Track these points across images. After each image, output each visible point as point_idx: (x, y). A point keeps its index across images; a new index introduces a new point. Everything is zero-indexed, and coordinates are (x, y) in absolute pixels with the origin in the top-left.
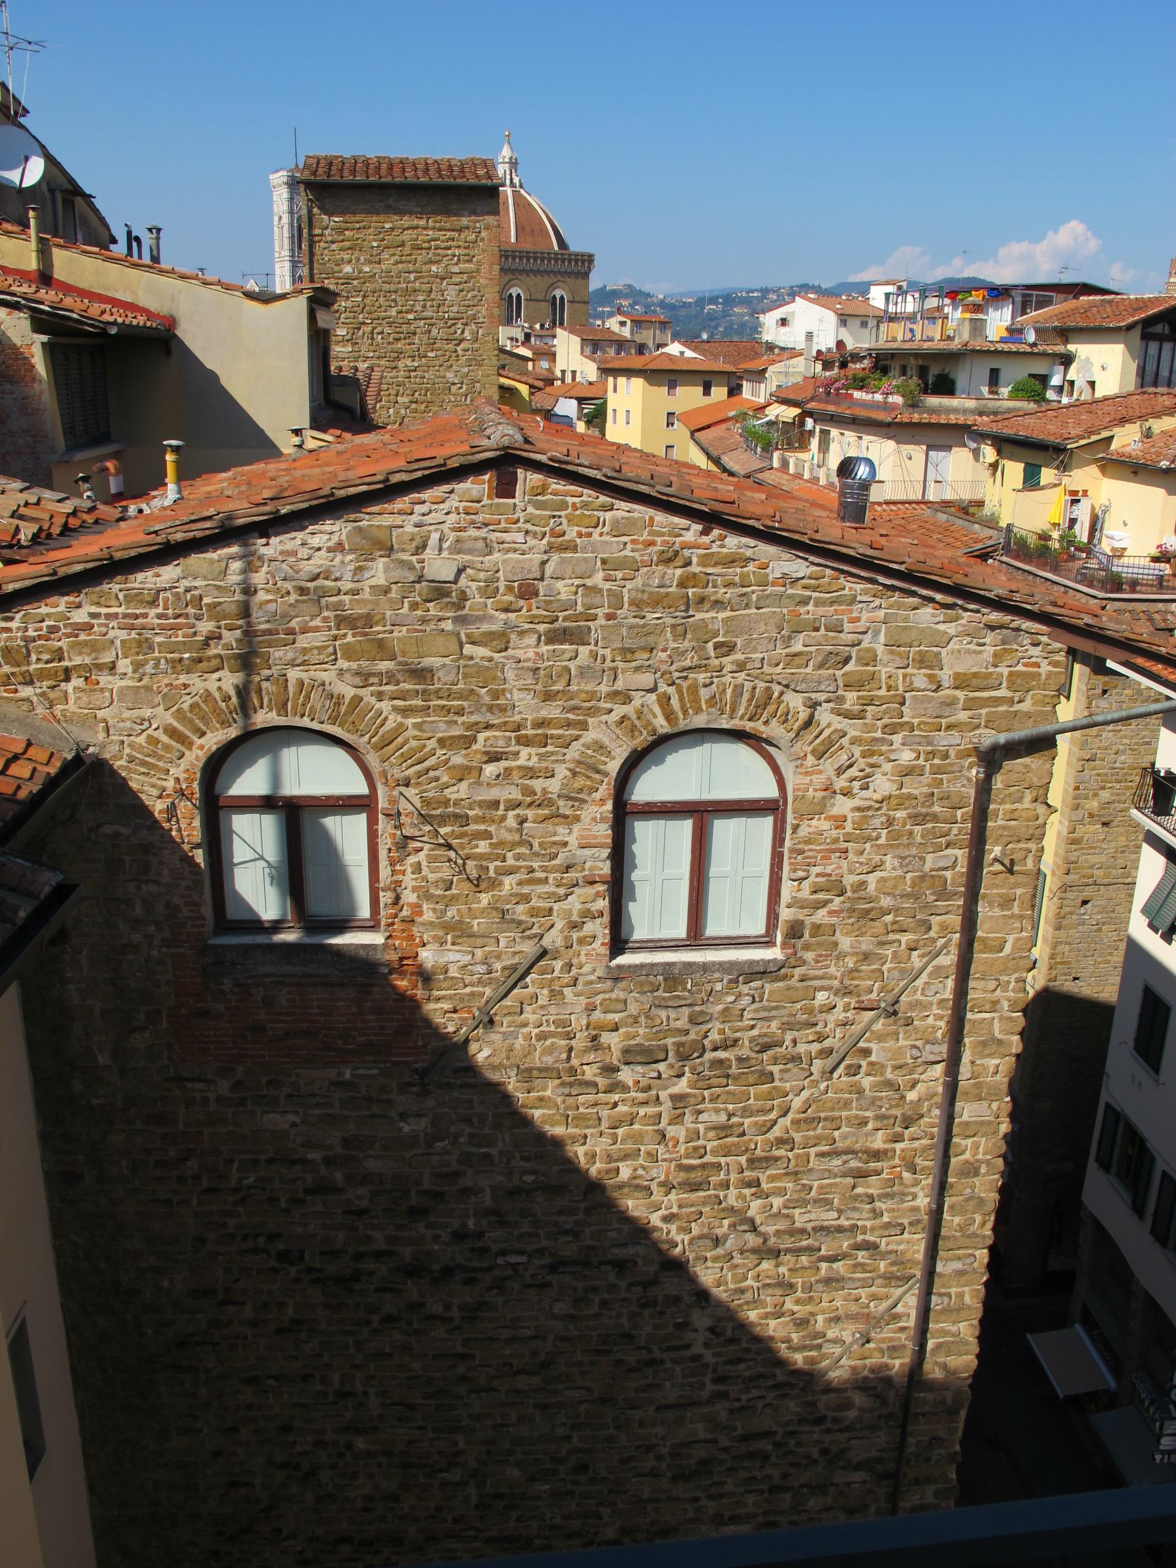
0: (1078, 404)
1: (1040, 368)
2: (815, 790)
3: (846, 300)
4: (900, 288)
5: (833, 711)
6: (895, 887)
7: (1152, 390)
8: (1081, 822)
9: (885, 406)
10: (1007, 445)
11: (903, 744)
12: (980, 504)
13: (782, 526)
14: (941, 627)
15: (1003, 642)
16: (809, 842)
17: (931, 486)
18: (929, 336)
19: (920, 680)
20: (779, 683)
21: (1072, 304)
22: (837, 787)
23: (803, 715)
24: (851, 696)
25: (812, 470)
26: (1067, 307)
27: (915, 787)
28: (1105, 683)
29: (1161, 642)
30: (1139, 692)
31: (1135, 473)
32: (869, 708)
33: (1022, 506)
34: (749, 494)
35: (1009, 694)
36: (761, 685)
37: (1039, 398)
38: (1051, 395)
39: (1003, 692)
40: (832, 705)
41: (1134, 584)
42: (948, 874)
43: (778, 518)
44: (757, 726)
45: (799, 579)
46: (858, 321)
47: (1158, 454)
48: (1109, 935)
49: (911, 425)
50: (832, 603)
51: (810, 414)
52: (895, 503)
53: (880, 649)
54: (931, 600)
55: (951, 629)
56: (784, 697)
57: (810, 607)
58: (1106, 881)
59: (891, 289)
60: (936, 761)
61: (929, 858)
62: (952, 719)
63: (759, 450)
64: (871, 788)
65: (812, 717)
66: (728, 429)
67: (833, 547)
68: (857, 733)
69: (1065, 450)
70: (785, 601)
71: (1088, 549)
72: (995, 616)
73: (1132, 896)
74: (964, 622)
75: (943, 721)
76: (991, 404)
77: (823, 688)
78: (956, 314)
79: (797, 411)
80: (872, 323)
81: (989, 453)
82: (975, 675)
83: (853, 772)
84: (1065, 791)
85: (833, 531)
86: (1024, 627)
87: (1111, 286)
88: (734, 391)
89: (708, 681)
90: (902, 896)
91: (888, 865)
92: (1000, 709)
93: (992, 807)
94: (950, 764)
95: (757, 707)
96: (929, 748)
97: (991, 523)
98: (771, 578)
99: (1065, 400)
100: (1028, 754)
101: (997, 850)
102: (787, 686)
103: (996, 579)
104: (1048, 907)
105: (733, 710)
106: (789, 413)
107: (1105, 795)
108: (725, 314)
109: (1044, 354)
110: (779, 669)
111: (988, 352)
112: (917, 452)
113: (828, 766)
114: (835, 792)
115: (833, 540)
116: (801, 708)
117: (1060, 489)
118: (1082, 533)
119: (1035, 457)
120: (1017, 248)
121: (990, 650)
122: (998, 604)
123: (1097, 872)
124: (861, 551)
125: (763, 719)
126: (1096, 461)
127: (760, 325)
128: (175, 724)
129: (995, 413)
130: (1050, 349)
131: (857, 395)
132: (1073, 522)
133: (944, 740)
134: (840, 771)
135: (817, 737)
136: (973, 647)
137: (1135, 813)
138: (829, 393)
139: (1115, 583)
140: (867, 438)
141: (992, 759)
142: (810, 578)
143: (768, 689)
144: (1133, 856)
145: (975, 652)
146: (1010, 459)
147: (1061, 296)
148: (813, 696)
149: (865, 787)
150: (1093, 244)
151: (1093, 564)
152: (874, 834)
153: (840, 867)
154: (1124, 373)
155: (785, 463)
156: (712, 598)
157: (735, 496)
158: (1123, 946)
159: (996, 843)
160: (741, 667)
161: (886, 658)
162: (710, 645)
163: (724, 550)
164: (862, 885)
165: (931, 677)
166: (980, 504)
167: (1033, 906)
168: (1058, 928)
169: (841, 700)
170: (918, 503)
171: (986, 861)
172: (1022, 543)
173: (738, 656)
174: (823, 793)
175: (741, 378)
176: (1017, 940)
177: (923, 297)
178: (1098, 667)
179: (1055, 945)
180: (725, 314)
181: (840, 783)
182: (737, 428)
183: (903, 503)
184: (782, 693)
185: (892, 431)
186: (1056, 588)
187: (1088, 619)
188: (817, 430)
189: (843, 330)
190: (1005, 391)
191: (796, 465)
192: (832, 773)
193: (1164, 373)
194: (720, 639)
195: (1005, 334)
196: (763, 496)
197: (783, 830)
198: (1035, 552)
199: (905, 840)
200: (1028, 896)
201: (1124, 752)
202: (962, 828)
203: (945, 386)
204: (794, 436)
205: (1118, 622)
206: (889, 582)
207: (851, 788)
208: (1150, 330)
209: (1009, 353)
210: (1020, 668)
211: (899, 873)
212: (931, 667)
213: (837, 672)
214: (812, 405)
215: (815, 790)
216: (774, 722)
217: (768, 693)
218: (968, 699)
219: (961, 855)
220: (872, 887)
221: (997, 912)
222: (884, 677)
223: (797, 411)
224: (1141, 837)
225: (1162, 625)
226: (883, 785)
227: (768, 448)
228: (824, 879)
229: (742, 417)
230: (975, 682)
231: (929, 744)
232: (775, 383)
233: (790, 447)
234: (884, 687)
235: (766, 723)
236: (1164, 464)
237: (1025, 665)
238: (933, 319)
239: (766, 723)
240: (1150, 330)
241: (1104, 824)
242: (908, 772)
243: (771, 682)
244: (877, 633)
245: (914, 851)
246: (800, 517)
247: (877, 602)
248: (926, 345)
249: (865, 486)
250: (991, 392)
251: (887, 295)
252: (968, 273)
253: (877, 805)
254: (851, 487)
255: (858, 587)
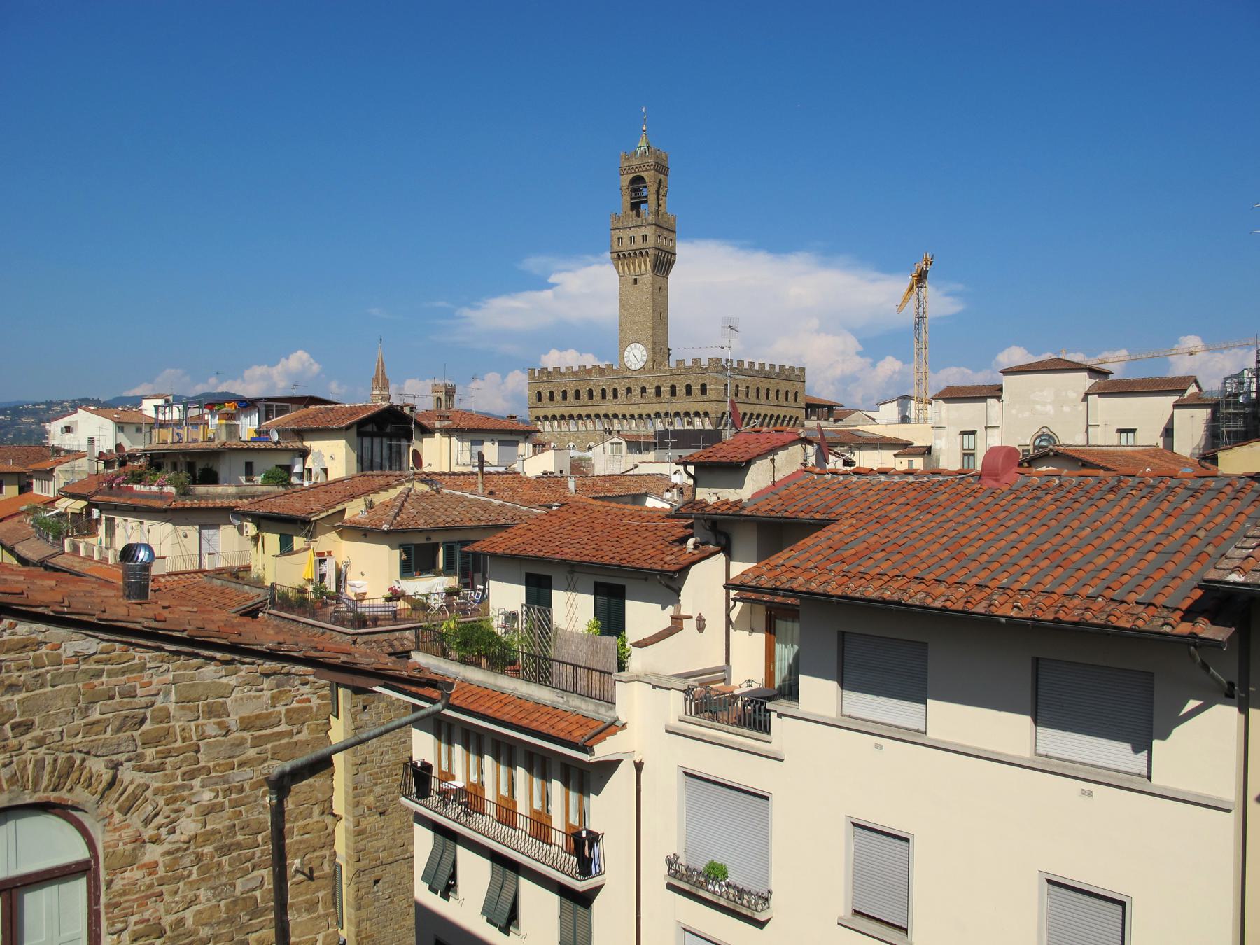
0: (316, 486)
1: (284, 460)
2: (125, 844)
3: (119, 409)
4: (167, 401)
5: (134, 768)
6: (211, 916)
7: (370, 473)
8: (363, 815)
9: (161, 496)
10: (265, 521)
11: (202, 787)
12: (248, 569)
13: (71, 610)
14: (224, 680)
15: (278, 686)
16: (124, 893)
17: (206, 558)
18: (194, 438)
19: (211, 728)
20: (80, 752)
21: (303, 412)
22: (146, 837)
23: (107, 776)
24: (150, 753)
25: (100, 553)
26: (300, 414)
27: (218, 823)
28: (364, 700)
29: (402, 667)
30: (392, 703)
31: (365, 535)
32: (167, 760)
33: (282, 568)
34: (39, 582)
35: (289, 728)
36: (62, 756)
37: (286, 483)
38: (294, 480)
39: (283, 727)
40: (133, 763)
41: (375, 620)
42: (258, 893)
43: (66, 603)
44: (63, 795)
45: (90, 656)
46: (133, 428)
47: (381, 520)
48: (400, 903)
49: (184, 510)
50: (124, 673)
51: (96, 505)
52: (176, 574)
53: (172, 707)
54: (213, 659)
55: (232, 681)
56: (87, 764)
57: (104, 679)
58: (390, 860)
59: (160, 402)
60: (234, 796)
61: (239, 883)
62: (243, 757)
63: (51, 538)
64: (178, 831)
65: (115, 777)
66: (21, 522)
67: (120, 624)
68: (160, 784)
69: (310, 522)
70: (79, 676)
71: (338, 597)
72: (268, 666)
73: (412, 867)
74: (243, 673)
75: (236, 761)
76: (248, 490)
77: (123, 749)
78: (214, 422)
79: (85, 503)
80: (145, 429)
81: (251, 529)
82: (258, 717)
83: (160, 820)
84: (347, 793)
85: (120, 609)
86: (293, 671)
87: (331, 398)
88: (25, 488)
89: (7, 761)
90: (219, 923)
91: (202, 898)
92: (283, 741)
93: (287, 826)
94: (246, 797)
95: (60, 777)
96: (226, 786)
97: (258, 583)
98: (64, 657)
99: (306, 484)
100: (311, 775)
101: (297, 862)
102: (88, 753)
103: (265, 633)
104: (347, 893)
105: (36, 783)
106: (77, 506)
107: (378, 790)
108: (13, 423)
109: (286, 450)
110: (79, 739)
111: (242, 449)
112: (192, 531)
113: (135, 819)
114: (144, 842)
115: (120, 618)
116: (104, 771)
117: (310, 553)
118: (330, 584)
119: (288, 529)
120: (258, 370)
121: (268, 694)
122: (270, 655)
123: (381, 855)
124: (146, 624)
125: (67, 787)
126: (335, 528)
127: (47, 432)
129: (253, 497)
130: (290, 446)
131: (136, 487)
132: (323, 577)
133: (238, 776)
134: (147, 822)
135: (122, 794)
136: (253, 693)
137: (403, 799)
138: (111, 487)
139: (361, 621)
140: (147, 523)
141: (281, 786)
142: (101, 653)
143: (70, 758)
144: (408, 835)
145: (255, 697)
146: (268, 532)
147: (295, 406)
148: (114, 758)
149: (173, 831)
150: (316, 368)
151: (342, 608)
152: (186, 873)
153: (157, 911)
154: (348, 461)
155: (76, 549)
156: (7, 683)
157: (24, 587)
158: (412, 910)
159: (296, 857)
160: (41, 742)
161: (178, 714)
162: (8, 727)
163: (16, 637)
164: (181, 922)
165: (219, 724)
166: (248, 569)
167: (335, 904)
168: (359, 908)
169: (141, 757)
170: (196, 572)
171: (289, 875)
172: (285, 597)
173: (38, 733)
174: (133, 845)
175: (31, 477)
176: (326, 937)
177: (186, 409)
178: (357, 691)
179: (358, 924)
180: (13, 423)
181: (149, 832)
182: (29, 520)
183: (183, 573)
184: (83, 761)
185: (169, 516)
186: (316, 630)
187: (344, 658)
188: (104, 518)
189: (121, 435)
190: (259, 479)
191: (86, 549)
192: (139, 825)
193: (377, 460)
194: (18, 719)
195: (255, 436)
196: (53, 583)
197: (97, 888)
198: (295, 603)
199: (215, 872)
200: (330, 896)
201: (387, 753)
202: (264, 851)
203: (210, 478)
204: (83, 525)
205: (368, 657)
206: (173, 648)
207: (159, 835)
208: (363, 429)
209: (259, 450)
210: (295, 705)
211: (214, 902)
212: (219, 716)
213: (135, 733)
214: (97, 498)
215: (125, 844)
216: (78, 789)
217: (70, 763)
218: (254, 738)
219: (266, 873)
220: (190, 922)
221: (306, 916)
222: (178, 731)
223: (85, 503)
224: (411, 818)
225: (401, 649)
226: (188, 826)
227: (59, 536)
228: (142, 926)
229: (34, 510)
230: (258, 723)
231: (226, 782)
232: (62, 481)
233: (80, 534)
234: (179, 740)
235: (71, 790)
236: (386, 527)
237: (298, 702)
238: (196, 425)
239: (71, 790)
240: (363, 429)
242: (210, 810)
243: (73, 751)
244: (167, 694)
245: (224, 880)
246: (87, 600)
247: (165, 667)
248: (192, 446)
249: (146, 567)
250: (247, 480)
251: (156, 407)
252: (222, 388)
253: (185, 846)
254: (133, 569)
255: (147, 656)
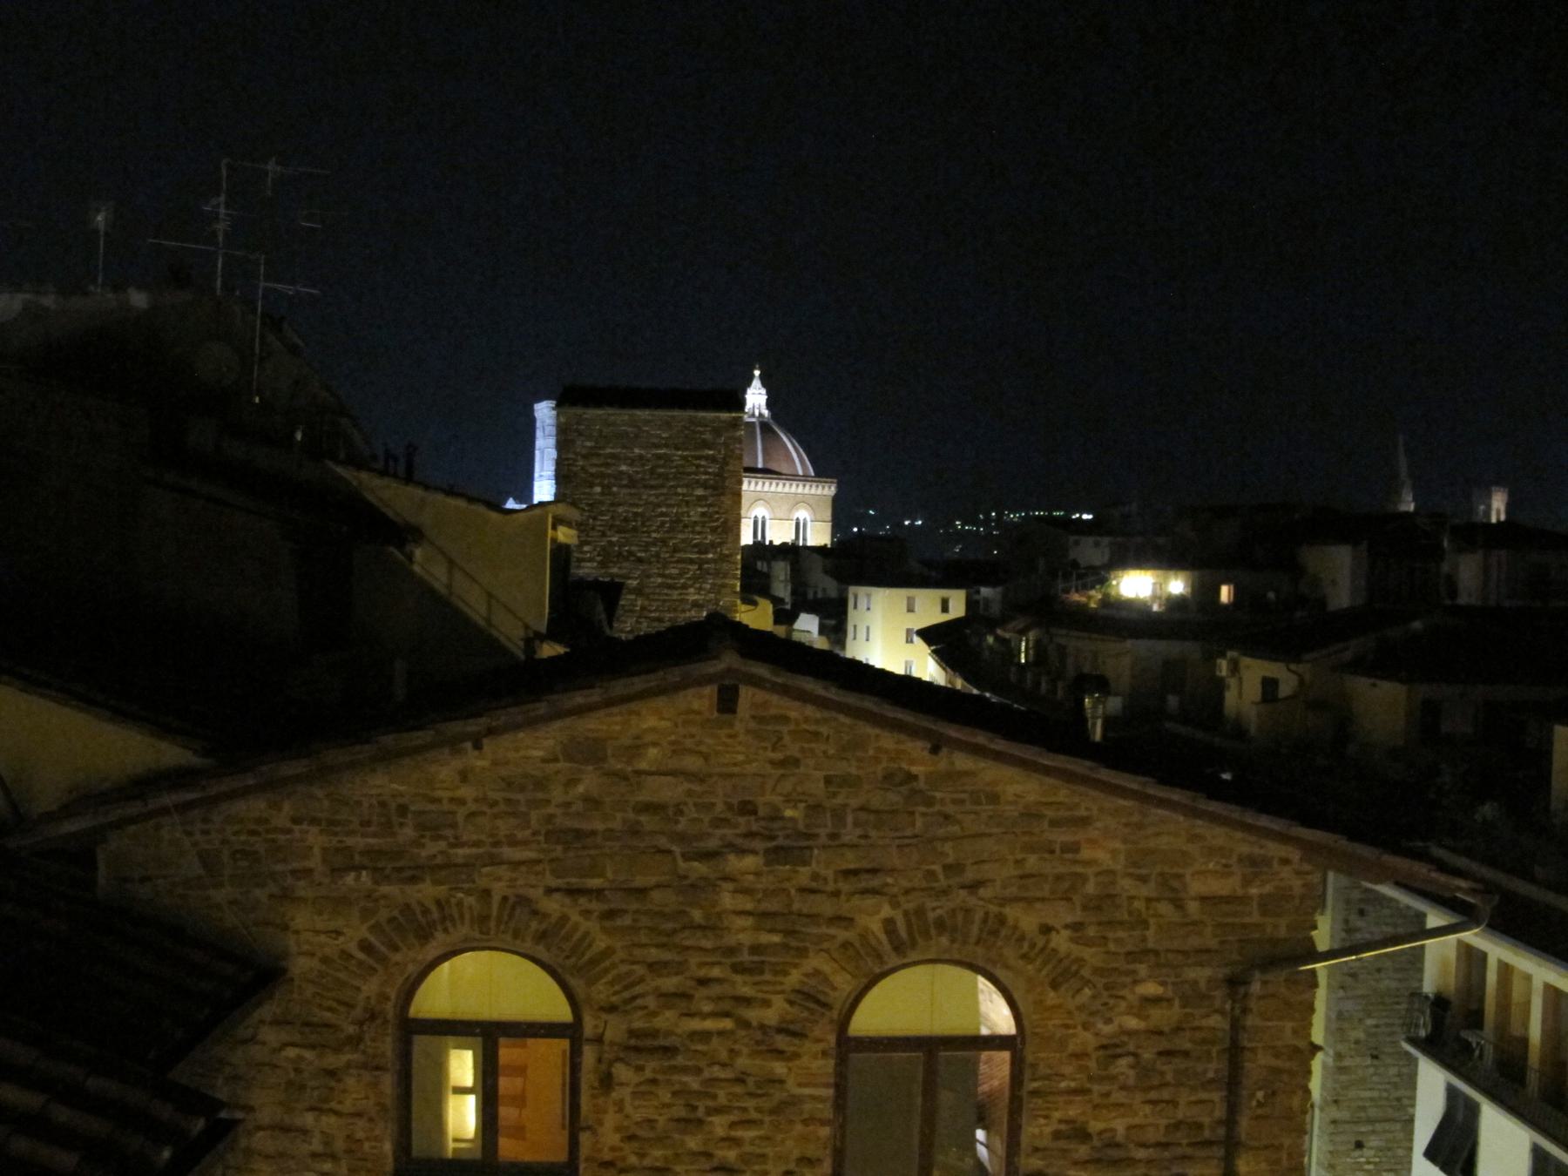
128: (372, 939)
241: (1375, 1057)
